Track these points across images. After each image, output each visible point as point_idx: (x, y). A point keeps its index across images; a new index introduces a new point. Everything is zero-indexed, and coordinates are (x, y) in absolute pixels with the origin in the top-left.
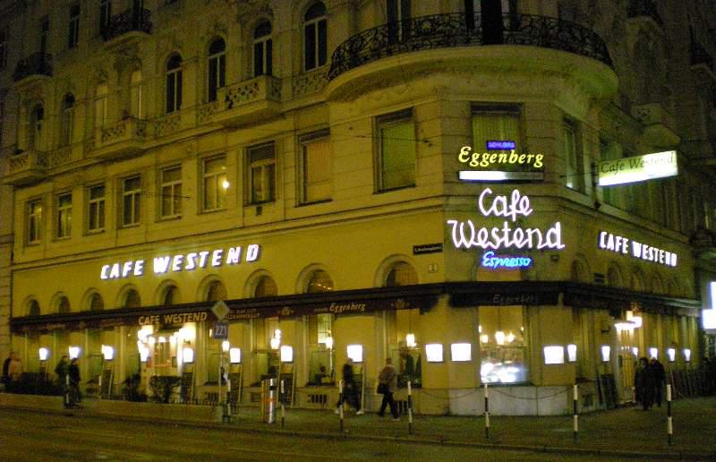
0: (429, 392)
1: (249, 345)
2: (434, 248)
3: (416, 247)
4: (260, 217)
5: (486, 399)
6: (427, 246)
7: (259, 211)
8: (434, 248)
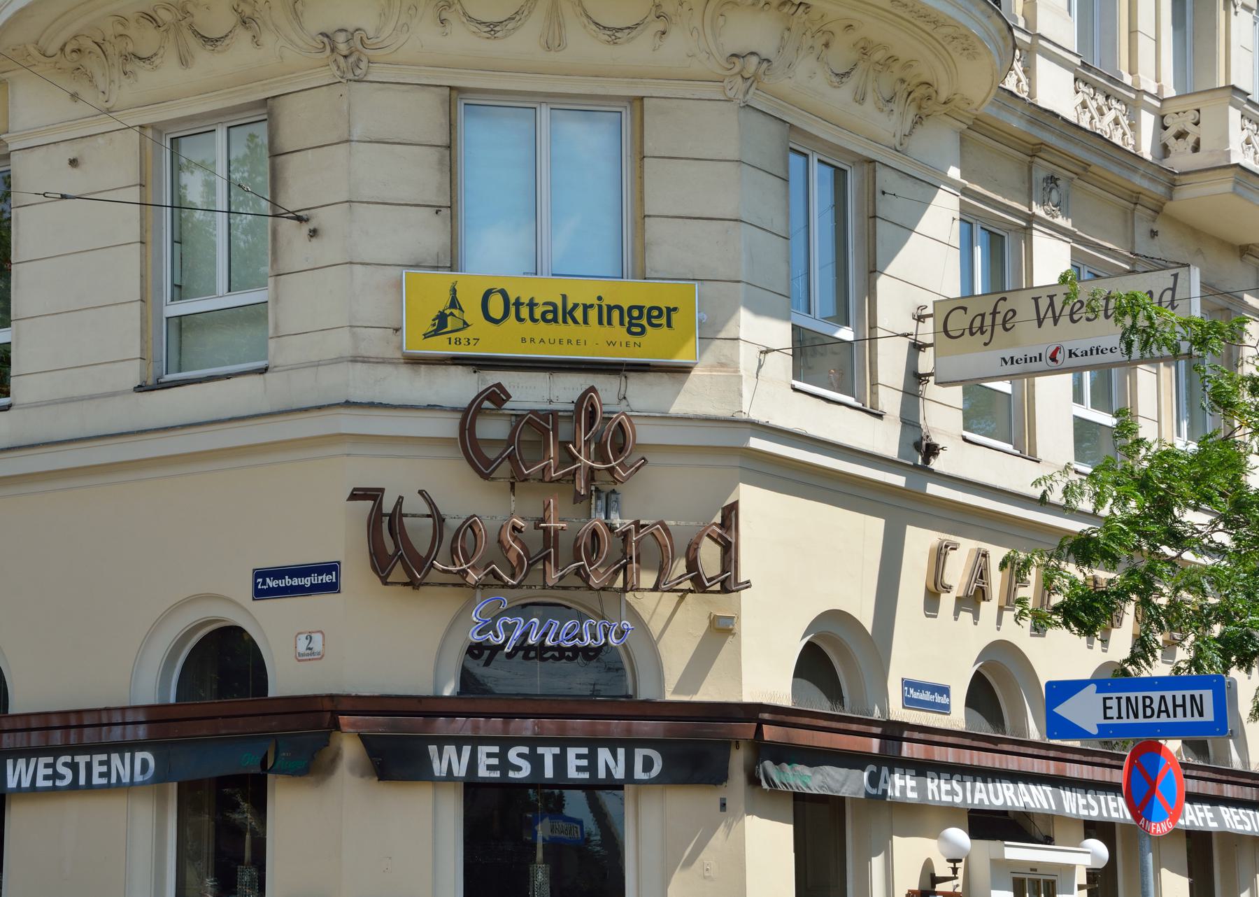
3: (260, 574)
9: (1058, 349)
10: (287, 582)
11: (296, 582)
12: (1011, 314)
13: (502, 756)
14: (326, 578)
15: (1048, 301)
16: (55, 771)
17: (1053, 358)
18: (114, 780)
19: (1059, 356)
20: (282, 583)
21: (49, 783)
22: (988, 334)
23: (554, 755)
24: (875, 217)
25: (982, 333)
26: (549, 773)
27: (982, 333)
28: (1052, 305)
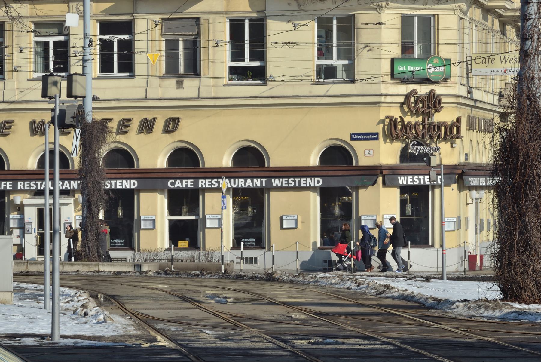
0: (362, 49)
1: (175, 358)
2: (371, 136)
3: (352, 134)
4: (180, 91)
5: (297, 252)
6: (364, 134)
7: (180, 84)
8: (371, 136)
9: (506, 70)
10: (362, 137)
11: (365, 137)
12: (493, 59)
13: (413, 179)
14: (374, 136)
15: (504, 57)
16: (288, 182)
17: (505, 72)
18: (308, 185)
19: (506, 72)
20: (360, 137)
21: (29, 188)
22: (487, 64)
23: (265, 181)
24: (463, 33)
25: (485, 63)
26: (297, 185)
27: (485, 63)
28: (505, 58)
